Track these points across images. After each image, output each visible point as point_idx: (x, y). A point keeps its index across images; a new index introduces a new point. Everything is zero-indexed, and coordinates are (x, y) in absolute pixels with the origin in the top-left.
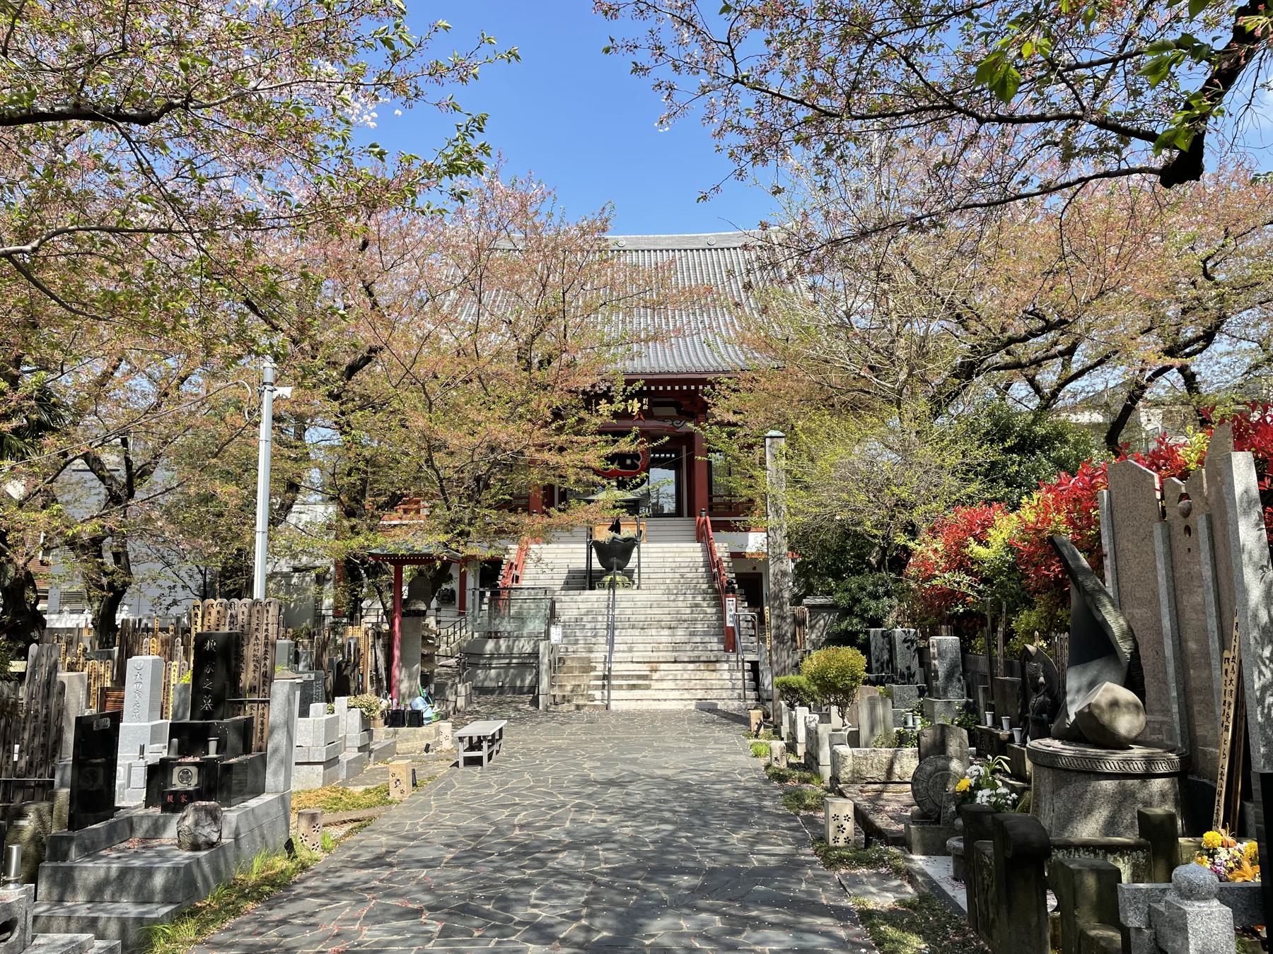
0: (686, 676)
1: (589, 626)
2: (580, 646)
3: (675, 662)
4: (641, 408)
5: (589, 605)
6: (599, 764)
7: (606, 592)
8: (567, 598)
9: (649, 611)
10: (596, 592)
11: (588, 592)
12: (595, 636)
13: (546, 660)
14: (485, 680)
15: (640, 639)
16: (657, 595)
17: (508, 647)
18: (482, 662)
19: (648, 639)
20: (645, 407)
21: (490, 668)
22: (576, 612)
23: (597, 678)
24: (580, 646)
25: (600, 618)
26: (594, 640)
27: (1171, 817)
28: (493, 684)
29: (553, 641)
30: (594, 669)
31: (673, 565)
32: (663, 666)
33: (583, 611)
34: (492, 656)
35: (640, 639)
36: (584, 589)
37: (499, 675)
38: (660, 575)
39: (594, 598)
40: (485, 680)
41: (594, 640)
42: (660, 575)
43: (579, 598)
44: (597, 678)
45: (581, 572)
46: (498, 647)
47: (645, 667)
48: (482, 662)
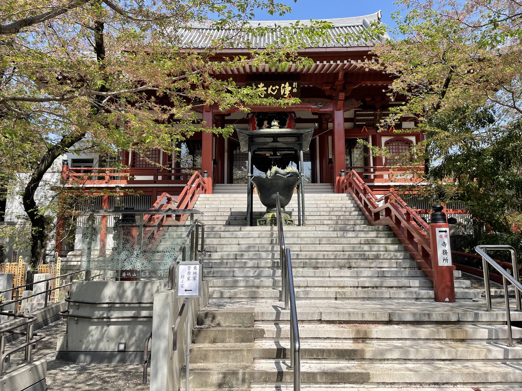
0: (425, 353)
1: (250, 264)
2: (240, 290)
3: (389, 322)
4: (291, 91)
5: (251, 241)
6: (226, 118)
7: (268, 228)
8: (227, 234)
9: (319, 248)
10: (258, 228)
11: (249, 228)
12: (258, 276)
13: (166, 330)
14: (99, 340)
15: (316, 281)
16: (324, 231)
17: (136, 291)
18: (97, 314)
19: (327, 281)
20: (295, 90)
21: (109, 324)
22: (235, 248)
23: (266, 354)
24: (240, 290)
25: (264, 255)
26: (257, 282)
27: (279, 281)
28: (112, 347)
29: (181, 293)
30: (260, 334)
31: (328, 209)
32: (377, 331)
33: (243, 247)
34: (112, 306)
35: (316, 281)
36: (245, 225)
37: (121, 333)
38: (317, 218)
39: (256, 234)
40: (99, 340)
41: (257, 282)
42: (317, 218)
43: (240, 234)
44: (266, 354)
45: (241, 213)
46: (121, 294)
47: (348, 331)
48: (97, 314)
